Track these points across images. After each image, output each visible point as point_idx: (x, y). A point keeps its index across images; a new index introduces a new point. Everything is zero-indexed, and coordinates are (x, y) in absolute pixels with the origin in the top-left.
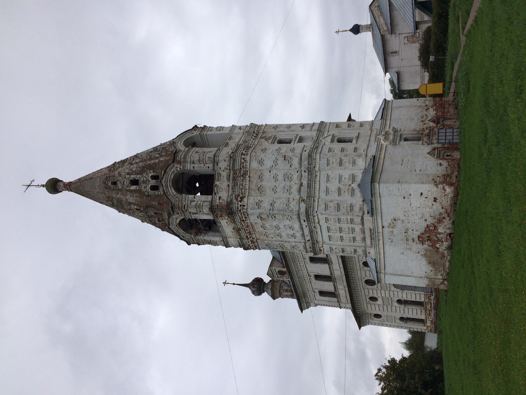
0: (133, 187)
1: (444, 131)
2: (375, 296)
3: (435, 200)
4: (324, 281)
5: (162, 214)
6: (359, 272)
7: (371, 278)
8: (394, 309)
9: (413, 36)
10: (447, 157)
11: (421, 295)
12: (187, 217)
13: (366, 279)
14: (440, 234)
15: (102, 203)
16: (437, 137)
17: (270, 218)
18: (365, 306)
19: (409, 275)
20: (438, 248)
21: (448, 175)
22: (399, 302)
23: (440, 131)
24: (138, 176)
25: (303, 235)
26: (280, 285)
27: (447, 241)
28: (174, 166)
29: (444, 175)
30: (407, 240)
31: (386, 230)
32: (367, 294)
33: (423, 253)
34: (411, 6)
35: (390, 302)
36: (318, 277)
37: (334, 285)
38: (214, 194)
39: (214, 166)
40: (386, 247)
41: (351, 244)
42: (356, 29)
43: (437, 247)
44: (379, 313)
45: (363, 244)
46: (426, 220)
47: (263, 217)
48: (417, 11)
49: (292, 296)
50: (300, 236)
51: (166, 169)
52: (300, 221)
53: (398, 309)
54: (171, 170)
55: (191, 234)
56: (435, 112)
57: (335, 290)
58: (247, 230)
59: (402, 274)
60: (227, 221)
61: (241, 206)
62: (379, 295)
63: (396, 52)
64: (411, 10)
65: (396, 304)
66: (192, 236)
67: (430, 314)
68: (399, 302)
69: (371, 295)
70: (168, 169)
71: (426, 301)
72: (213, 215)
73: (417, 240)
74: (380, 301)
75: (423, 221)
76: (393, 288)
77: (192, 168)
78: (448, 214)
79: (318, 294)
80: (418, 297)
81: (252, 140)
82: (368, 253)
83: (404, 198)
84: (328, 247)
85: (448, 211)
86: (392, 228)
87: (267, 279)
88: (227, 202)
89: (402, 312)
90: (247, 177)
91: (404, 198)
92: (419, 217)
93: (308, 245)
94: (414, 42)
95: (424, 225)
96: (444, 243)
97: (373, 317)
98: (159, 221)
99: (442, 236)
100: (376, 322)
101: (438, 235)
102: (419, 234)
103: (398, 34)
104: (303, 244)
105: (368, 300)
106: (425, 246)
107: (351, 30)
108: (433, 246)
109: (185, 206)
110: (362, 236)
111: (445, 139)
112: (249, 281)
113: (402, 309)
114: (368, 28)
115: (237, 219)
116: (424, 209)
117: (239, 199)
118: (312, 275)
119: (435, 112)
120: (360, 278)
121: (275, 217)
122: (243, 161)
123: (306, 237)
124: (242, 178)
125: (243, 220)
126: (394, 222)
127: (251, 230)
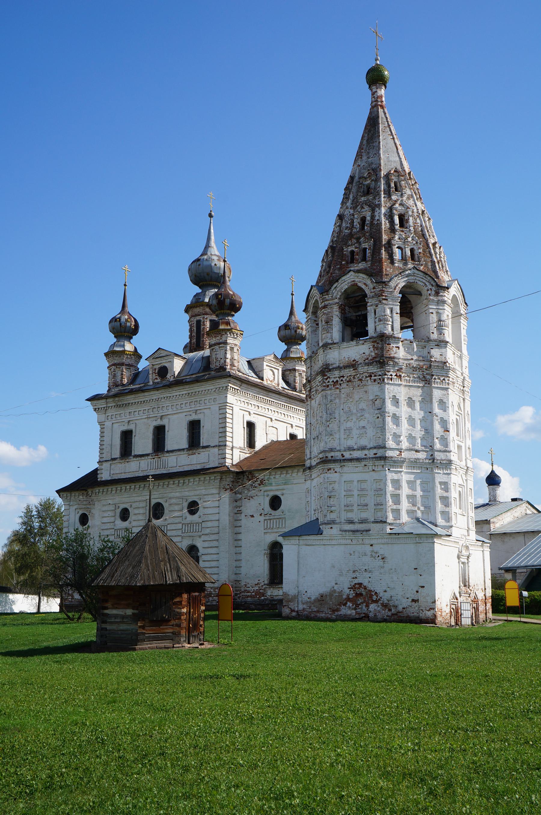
2: (132, 517)
4: (153, 440)
6: (178, 494)
12: (370, 301)
13: (166, 505)
14: (367, 606)
16: (465, 601)
20: (345, 605)
24: (412, 228)
25: (351, 449)
27: (356, 613)
28: (432, 286)
30: (354, 572)
31: (369, 548)
32: (134, 505)
37: (147, 455)
39: (435, 341)
40: (342, 547)
43: (346, 603)
45: (343, 521)
46: (385, 591)
47: (376, 402)
49: (114, 384)
50: (348, 444)
51: (430, 276)
55: (339, 299)
57: (136, 456)
58: (354, 378)
60: (367, 354)
61: (391, 375)
66: (337, 301)
70: (429, 278)
73: (356, 581)
75: (385, 589)
77: (431, 311)
78: (396, 614)
79: (125, 428)
82: (330, 526)
85: (400, 614)
88: (394, 358)
93: (338, 455)
96: (354, 611)
97: (81, 512)
101: (365, 604)
102: (365, 584)
104: (338, 448)
106: (347, 591)
107: (493, 472)
108: (348, 599)
109: (387, 300)
115: (372, 369)
118: (165, 422)
122: (442, 379)
126: (380, 558)
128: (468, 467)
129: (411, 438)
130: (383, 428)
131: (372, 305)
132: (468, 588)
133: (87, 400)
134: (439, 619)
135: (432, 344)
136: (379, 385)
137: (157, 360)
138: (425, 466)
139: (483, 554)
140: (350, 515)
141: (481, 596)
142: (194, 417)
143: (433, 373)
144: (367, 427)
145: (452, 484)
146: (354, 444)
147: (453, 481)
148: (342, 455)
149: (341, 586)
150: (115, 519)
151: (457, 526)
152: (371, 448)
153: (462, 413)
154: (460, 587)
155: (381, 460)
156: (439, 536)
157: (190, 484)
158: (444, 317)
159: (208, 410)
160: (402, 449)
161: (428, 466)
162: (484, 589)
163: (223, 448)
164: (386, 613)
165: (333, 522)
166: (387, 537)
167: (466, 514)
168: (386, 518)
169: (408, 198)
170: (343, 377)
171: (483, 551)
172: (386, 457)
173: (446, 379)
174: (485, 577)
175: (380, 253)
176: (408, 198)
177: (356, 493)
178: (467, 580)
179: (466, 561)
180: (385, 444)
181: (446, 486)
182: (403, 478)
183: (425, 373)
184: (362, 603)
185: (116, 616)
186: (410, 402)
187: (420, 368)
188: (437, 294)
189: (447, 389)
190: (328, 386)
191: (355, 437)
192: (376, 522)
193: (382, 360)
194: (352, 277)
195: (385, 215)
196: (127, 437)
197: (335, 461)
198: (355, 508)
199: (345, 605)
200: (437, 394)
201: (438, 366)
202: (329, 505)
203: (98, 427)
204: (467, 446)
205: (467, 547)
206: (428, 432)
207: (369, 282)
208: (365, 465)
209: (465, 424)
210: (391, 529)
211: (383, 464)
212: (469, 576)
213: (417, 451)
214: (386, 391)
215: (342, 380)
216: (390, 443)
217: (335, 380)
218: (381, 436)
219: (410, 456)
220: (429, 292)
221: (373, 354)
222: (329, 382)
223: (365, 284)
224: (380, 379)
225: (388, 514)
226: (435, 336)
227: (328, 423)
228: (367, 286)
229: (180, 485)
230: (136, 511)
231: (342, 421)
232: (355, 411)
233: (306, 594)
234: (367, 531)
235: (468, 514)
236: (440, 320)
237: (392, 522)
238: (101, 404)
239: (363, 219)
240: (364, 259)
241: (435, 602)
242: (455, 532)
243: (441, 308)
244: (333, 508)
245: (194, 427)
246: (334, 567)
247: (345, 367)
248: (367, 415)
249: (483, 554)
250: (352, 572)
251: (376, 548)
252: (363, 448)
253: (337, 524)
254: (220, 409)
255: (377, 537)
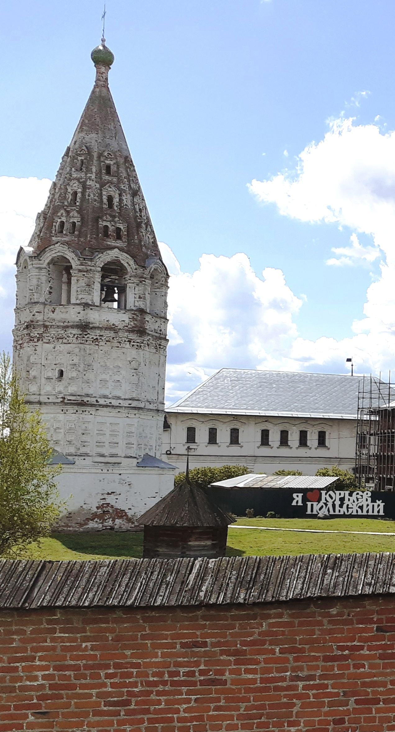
14: (114, 520)
25: (105, 397)
27: (103, 526)
46: (130, 509)
82: (84, 458)
93: (93, 400)
96: (101, 525)
101: (111, 519)
106: (96, 510)
115: (132, 336)
126: (127, 484)
136: (137, 350)
140: (100, 450)
146: (108, 394)
148: (97, 400)
165: (87, 455)
170: (102, 336)
177: (108, 433)
184: (109, 518)
185: (194, 546)
190: (87, 341)
194: (116, 253)
197: (92, 405)
198: (107, 444)
199: (92, 520)
215: (101, 339)
217: (95, 338)
223: (128, 263)
227: (85, 373)
228: (129, 265)
234: (118, 463)
239: (110, 199)
240: (119, 237)
247: (106, 329)
252: (119, 398)
253: (89, 456)
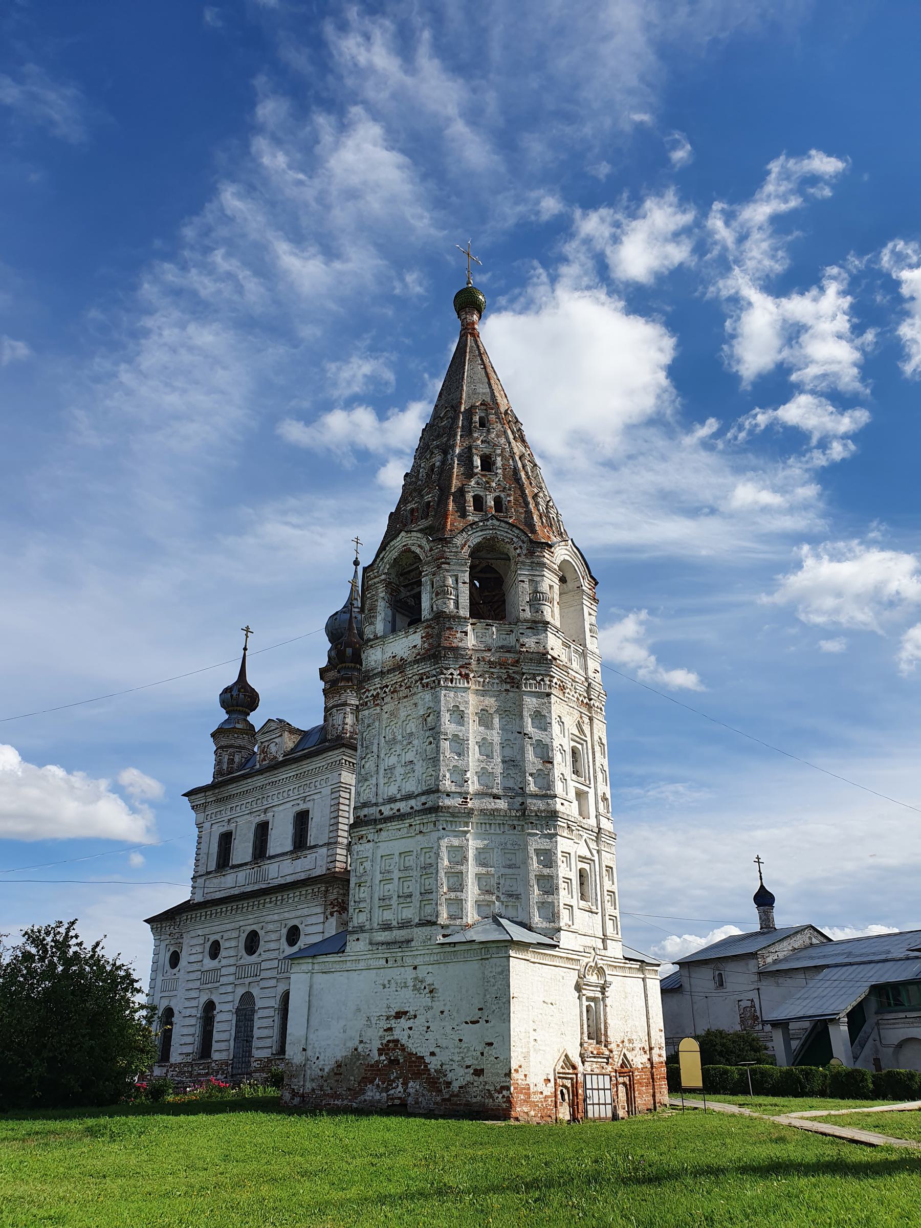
0: (477, 462)
1: (607, 1086)
2: (223, 953)
3: (478, 1072)
5: (426, 517)
6: (276, 917)
7: (262, 943)
8: (194, 994)
9: (755, 1018)
10: (559, 1093)
11: (225, 1053)
14: (405, 1084)
15: (440, 395)
16: (597, 1071)
17: (428, 734)
18: (200, 932)
19: (311, 1023)
20: (372, 1082)
21: (528, 1095)
22: (210, 1006)
23: (607, 1078)
24: (499, 471)
25: (392, 800)
26: (244, 748)
28: (524, 543)
29: (529, 1089)
33: (360, 1050)
34: (819, 1012)
35: (209, 986)
36: (262, 830)
37: (246, 864)
38: (474, 620)
39: (526, 621)
41: (376, 900)
42: (764, 899)
44: (183, 962)
46: (433, 1054)
47: (429, 719)
48: (807, 1025)
49: (218, 773)
52: (423, 794)
53: (194, 1003)
54: (517, 537)
56: (640, 1066)
57: (234, 867)
59: (313, 1010)
60: (419, 646)
61: (452, 674)
62: (224, 962)
63: (721, 984)
64: (810, 1013)
65: (204, 998)
66: (383, 577)
67: (182, 1073)
68: (210, 1006)
69: (224, 944)
71: (213, 1065)
72: (432, 619)
74: (209, 964)
76: (281, 988)
78: (449, 1100)
79: (224, 829)
80: (223, 1046)
81: (576, 695)
82: (356, 936)
83: (480, 1009)
84: (369, 854)
86: (414, 986)
87: (257, 719)
88: (458, 648)
89: (188, 1012)
90: (508, 687)
91: (480, 1009)
92: (439, 1041)
94: (742, 1022)
95: (423, 1051)
97: (172, 949)
98: (412, 510)
99: (400, 1088)
100: (161, 956)
102: (403, 1042)
103: (759, 985)
104: (374, 801)
105: (213, 938)
107: (762, 887)
109: (449, 564)
110: (395, 923)
111: (592, 1089)
112: (251, 680)
113: (194, 1012)
114: (767, 924)
116: (457, 1050)
117: (464, 671)
119: (640, 1066)
120: (262, 919)
121: (430, 743)
122: (539, 678)
123: (388, 807)
124: (505, 676)
125: (422, 679)
126: (427, 990)
127: (401, 694)
128: (600, 829)
129: (483, 774)
130: (434, 761)
131: (427, 575)
132: (605, 1046)
133: (184, 795)
134: (519, 1109)
135: (522, 627)
137: (267, 735)
138: (510, 823)
139: (645, 986)
140: (388, 915)
141: (639, 1060)
142: (303, 807)
143: (524, 671)
144: (415, 761)
145: (559, 854)
147: (560, 849)
148: (380, 811)
149: (367, 1046)
150: (203, 957)
151: (573, 928)
152: (417, 795)
153: (589, 739)
154: (581, 1045)
155: (430, 813)
156: (524, 946)
157: (290, 901)
158: (544, 587)
159: (318, 796)
160: (468, 793)
161: (515, 823)
162: (647, 1048)
163: (333, 846)
164: (430, 1099)
166: (437, 951)
167: (600, 910)
168: (437, 917)
169: (498, 436)
171: (644, 979)
172: (439, 807)
173: (547, 679)
174: (649, 1026)
175: (447, 504)
176: (498, 436)
178: (603, 1032)
179: (599, 995)
180: (438, 785)
181: (548, 858)
182: (470, 842)
183: (511, 671)
184: (398, 1078)
186: (484, 718)
187: (502, 664)
188: (531, 553)
189: (549, 695)
191: (399, 779)
192: (421, 924)
193: (438, 654)
195: (460, 455)
196: (226, 839)
200: (530, 703)
201: (531, 659)
202: (357, 900)
203: (196, 831)
204: (600, 794)
205: (601, 971)
206: (513, 764)
207: (424, 542)
208: (411, 825)
209: (594, 758)
210: (444, 936)
211: (434, 819)
212: (606, 1023)
213: (496, 797)
214: (442, 698)
216: (447, 784)
218: (433, 773)
219: (483, 806)
220: (518, 551)
221: (426, 645)
222: (367, 697)
224: (434, 681)
225: (439, 908)
226: (528, 615)
227: (363, 761)
229: (278, 903)
230: (227, 944)
231: (382, 756)
232: (400, 738)
233: (317, 1062)
235: (603, 909)
236: (536, 592)
237: (447, 922)
238: (200, 799)
241: (508, 1074)
242: (566, 940)
243: (537, 573)
244: (362, 905)
245: (302, 819)
246: (359, 1010)
248: (416, 742)
249: (645, 986)
250: (385, 1018)
251: (422, 972)
252: (408, 797)
254: (332, 793)
255: (423, 952)
